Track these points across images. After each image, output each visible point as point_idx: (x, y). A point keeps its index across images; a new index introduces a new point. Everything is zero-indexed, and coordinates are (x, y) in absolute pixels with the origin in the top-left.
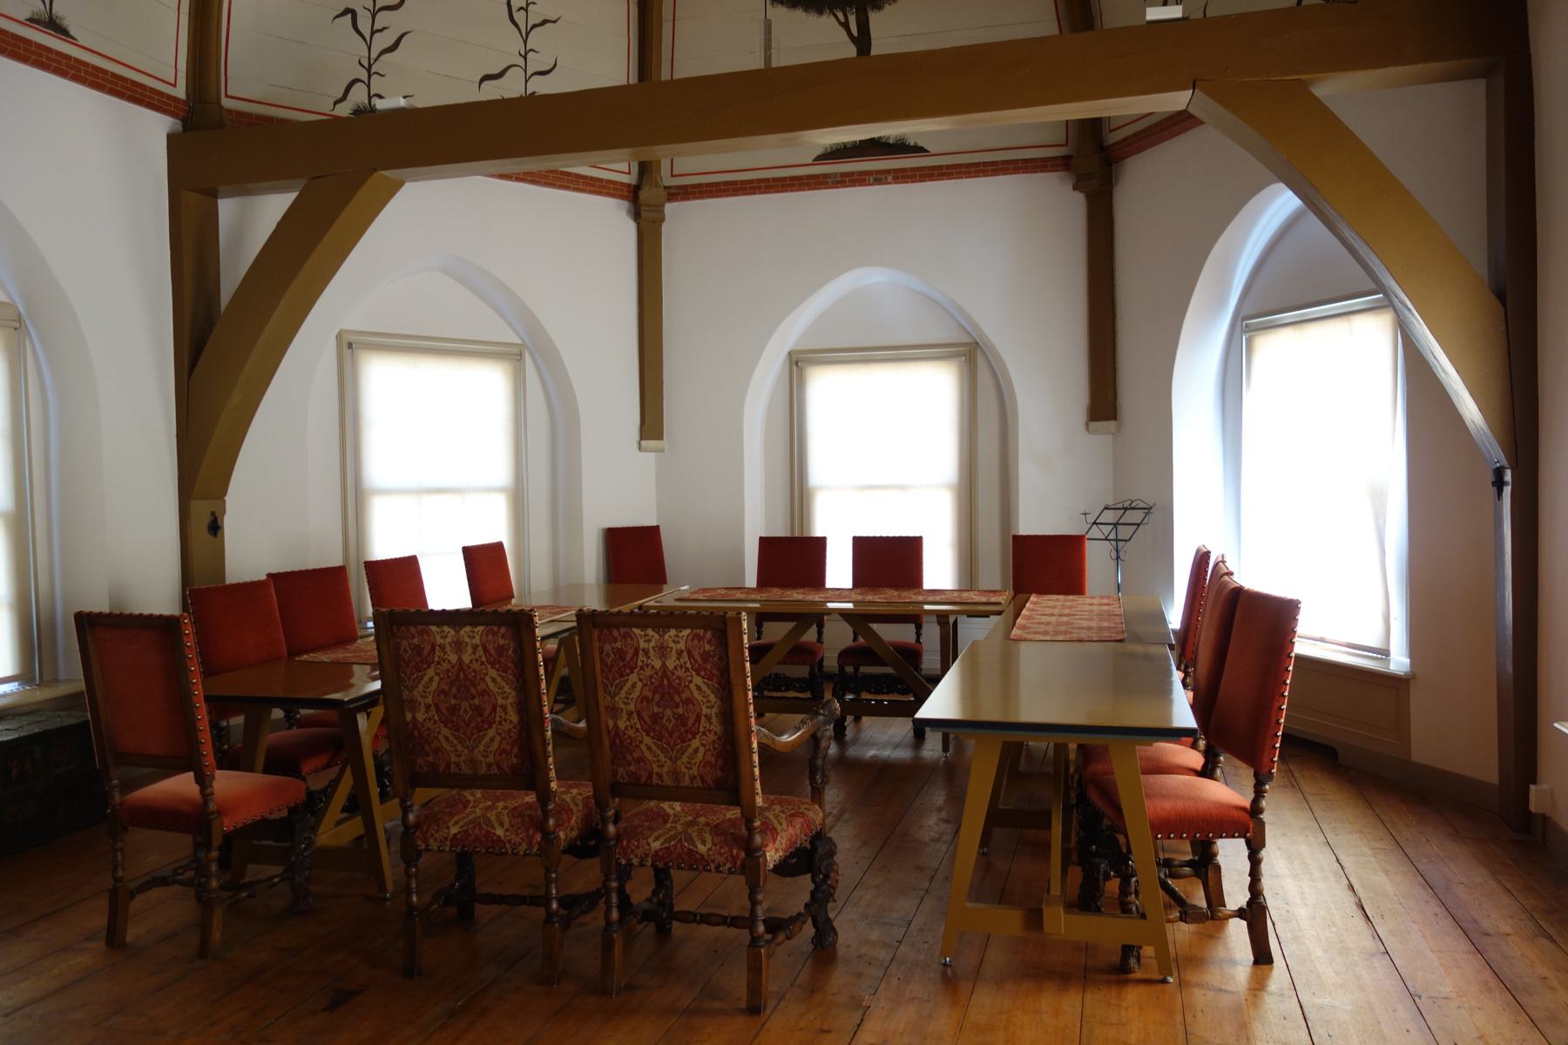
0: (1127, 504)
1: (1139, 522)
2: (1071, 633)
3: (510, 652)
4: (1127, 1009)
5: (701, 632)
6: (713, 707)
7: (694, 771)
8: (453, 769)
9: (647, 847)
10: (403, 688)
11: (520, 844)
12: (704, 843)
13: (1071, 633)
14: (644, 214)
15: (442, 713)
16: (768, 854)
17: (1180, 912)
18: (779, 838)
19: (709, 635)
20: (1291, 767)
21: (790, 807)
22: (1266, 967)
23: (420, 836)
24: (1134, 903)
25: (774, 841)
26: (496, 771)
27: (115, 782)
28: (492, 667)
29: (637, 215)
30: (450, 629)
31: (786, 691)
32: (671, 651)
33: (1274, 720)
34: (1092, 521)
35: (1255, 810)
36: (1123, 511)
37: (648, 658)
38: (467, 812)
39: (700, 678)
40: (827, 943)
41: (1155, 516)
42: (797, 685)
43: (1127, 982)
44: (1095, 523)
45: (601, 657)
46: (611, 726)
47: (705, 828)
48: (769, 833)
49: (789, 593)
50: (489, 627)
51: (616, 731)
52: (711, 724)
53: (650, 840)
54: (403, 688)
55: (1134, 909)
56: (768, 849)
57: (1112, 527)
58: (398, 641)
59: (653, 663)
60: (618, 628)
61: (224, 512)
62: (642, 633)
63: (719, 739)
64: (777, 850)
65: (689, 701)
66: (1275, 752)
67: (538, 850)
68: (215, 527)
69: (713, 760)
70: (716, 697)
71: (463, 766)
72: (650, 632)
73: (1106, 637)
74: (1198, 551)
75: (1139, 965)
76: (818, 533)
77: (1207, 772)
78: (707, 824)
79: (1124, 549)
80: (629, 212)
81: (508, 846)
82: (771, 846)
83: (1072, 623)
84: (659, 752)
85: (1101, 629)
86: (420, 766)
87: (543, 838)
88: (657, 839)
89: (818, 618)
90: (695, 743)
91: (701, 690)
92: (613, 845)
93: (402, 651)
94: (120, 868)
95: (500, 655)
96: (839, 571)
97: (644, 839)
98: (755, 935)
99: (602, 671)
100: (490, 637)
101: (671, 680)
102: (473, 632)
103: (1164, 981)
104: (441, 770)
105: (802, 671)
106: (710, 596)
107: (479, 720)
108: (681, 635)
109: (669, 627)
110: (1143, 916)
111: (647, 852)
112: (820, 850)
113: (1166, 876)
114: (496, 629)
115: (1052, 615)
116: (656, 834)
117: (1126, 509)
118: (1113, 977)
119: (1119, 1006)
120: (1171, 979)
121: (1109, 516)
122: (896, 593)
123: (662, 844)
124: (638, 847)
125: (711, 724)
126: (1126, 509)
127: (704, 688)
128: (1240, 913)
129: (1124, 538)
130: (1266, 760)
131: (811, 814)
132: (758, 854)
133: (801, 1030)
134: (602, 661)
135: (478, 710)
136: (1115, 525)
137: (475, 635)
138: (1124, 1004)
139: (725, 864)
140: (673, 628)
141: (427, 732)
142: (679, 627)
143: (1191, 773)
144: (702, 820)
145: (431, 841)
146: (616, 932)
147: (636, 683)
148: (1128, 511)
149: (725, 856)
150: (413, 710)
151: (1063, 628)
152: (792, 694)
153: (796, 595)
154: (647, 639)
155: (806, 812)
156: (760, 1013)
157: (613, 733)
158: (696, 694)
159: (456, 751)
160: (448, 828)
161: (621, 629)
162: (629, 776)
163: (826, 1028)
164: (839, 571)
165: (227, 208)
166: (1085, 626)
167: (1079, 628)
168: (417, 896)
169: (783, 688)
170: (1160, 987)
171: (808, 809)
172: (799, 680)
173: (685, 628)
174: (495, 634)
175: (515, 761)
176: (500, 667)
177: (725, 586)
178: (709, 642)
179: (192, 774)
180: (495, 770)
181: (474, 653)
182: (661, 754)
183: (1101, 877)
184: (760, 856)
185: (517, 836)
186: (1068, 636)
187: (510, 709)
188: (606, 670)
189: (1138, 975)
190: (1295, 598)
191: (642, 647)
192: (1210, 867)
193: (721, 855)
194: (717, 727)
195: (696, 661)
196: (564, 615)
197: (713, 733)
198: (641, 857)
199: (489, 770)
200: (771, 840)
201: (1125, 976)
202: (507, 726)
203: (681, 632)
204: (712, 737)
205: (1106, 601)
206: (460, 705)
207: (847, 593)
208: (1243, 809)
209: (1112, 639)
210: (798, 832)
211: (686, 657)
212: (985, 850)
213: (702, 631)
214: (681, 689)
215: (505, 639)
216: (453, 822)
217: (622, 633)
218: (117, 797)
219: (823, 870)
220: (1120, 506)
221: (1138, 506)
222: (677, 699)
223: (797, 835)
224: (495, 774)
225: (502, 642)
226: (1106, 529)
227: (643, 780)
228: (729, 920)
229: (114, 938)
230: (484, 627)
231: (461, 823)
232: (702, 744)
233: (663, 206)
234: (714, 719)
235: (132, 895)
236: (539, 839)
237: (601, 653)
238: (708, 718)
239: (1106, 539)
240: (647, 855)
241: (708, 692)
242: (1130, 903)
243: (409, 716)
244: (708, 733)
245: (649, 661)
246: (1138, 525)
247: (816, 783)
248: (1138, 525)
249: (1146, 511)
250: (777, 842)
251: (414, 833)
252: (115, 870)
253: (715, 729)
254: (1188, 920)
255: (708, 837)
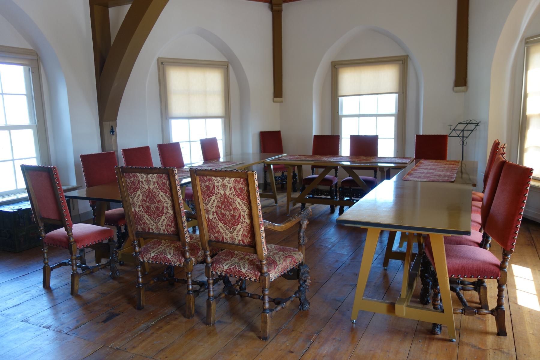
0: (468, 122)
1: (473, 129)
2: (431, 177)
3: (167, 185)
4: (430, 354)
5: (239, 179)
6: (245, 212)
7: (240, 238)
8: (151, 231)
9: (222, 268)
10: (130, 198)
11: (177, 262)
12: (244, 268)
13: (431, 177)
14: (274, 8)
15: (144, 209)
16: (271, 275)
17: (462, 310)
18: (277, 267)
19: (242, 181)
20: (533, 236)
21: (287, 253)
22: (503, 337)
23: (140, 256)
24: (439, 305)
25: (275, 268)
26: (167, 232)
27: (41, 228)
28: (161, 191)
29: (272, 9)
30: (144, 175)
31: (321, 195)
32: (227, 187)
33: (514, 225)
34: (453, 129)
35: (501, 267)
36: (466, 125)
37: (219, 189)
38: (159, 247)
39: (147, 215)
40: (305, 308)
41: (481, 127)
42: (325, 193)
43: (433, 339)
44: (454, 130)
45: (201, 188)
46: (207, 217)
47: (246, 261)
48: (273, 265)
49: (323, 157)
50: (158, 175)
51: (209, 219)
52: (245, 219)
53: (224, 265)
54: (130, 198)
55: (439, 307)
56: (271, 272)
57: (461, 131)
58: (126, 179)
59: (220, 192)
60: (206, 176)
61: (116, 126)
62: (216, 179)
63: (248, 225)
64: (276, 273)
65: (235, 209)
66: (515, 241)
67: (183, 265)
68: (113, 131)
69: (246, 234)
70: (246, 207)
71: (154, 230)
72: (218, 178)
73: (446, 180)
74: (495, 142)
75: (441, 331)
76: (174, 140)
77: (482, 245)
78: (248, 259)
79: (465, 141)
80: (269, 7)
81: (172, 263)
82: (273, 271)
83: (433, 173)
84: (225, 229)
85: (445, 176)
86: (139, 229)
87: (185, 261)
88: (227, 265)
89: (335, 167)
90: (239, 226)
91: (240, 204)
92: (210, 266)
93: (128, 183)
94: (46, 259)
95: (164, 186)
96: (345, 149)
97: (222, 264)
98: (264, 308)
99: (202, 194)
100: (159, 179)
101: (228, 199)
102: (152, 176)
103: (451, 341)
104: (147, 231)
105: (326, 188)
106: (292, 158)
107: (158, 212)
108: (231, 180)
109: (226, 177)
110: (443, 312)
111: (223, 270)
112: (302, 270)
113: (460, 290)
114: (161, 175)
115: (426, 169)
116: (227, 262)
117: (468, 124)
118: (428, 336)
119: (427, 352)
120: (454, 340)
121: (461, 127)
122: (365, 158)
123: (228, 267)
124: (219, 267)
125: (245, 219)
126: (468, 124)
127: (241, 203)
128: (492, 312)
129: (466, 136)
130: (509, 244)
131: (296, 256)
132: (266, 275)
133: (281, 350)
134: (201, 190)
135: (157, 208)
136: (463, 131)
137: (154, 177)
138: (429, 351)
139: (252, 278)
140: (227, 177)
141: (140, 216)
142: (230, 177)
143: (476, 244)
144: (247, 257)
145: (145, 259)
146: (212, 300)
147: (214, 200)
148: (469, 125)
149: (253, 274)
150: (134, 207)
151: (428, 175)
152: (323, 197)
153: (325, 159)
154: (217, 181)
155: (294, 255)
156: (266, 340)
157: (207, 220)
158: (238, 205)
159: (151, 224)
160: (150, 254)
161: (207, 177)
162: (215, 238)
163: (292, 350)
164: (345, 149)
165: (112, 11)
166: (438, 174)
167: (435, 175)
168: (139, 281)
169: (320, 194)
170: (449, 343)
171: (295, 254)
172: (326, 191)
173: (232, 177)
174: (161, 177)
175: (173, 229)
176: (164, 191)
177: (299, 155)
178: (242, 184)
179: (64, 228)
180: (166, 232)
181: (230, 190)
182: (226, 230)
183: (430, 288)
184: (266, 276)
185: (175, 259)
186: (429, 179)
187: (169, 208)
188: (203, 194)
189: (439, 336)
190: (530, 167)
191: (216, 185)
192: (481, 287)
193: (251, 274)
194: (248, 221)
195: (237, 192)
196: (230, 166)
197: (246, 222)
198: (221, 272)
199: (164, 232)
200: (273, 269)
201: (433, 336)
202: (169, 215)
203: (231, 179)
204: (245, 224)
205: (453, 163)
206: (150, 206)
207: (345, 158)
208: (496, 265)
209: (448, 181)
210: (288, 264)
211: (233, 190)
212: (386, 268)
213: (239, 179)
214: (141, 219)
215: (165, 180)
216: (152, 251)
217: (208, 179)
218: (43, 234)
219: (303, 279)
220: (465, 122)
221: (473, 123)
222: (231, 208)
223: (288, 265)
224: (166, 234)
225: (164, 181)
226: (458, 132)
227: (220, 240)
228: (261, 297)
229: (46, 285)
230: (157, 174)
231: (156, 252)
232: (242, 227)
233: (282, 4)
234: (246, 217)
235: (52, 269)
236: (183, 261)
237: (201, 187)
238: (244, 216)
239: (458, 136)
240: (223, 271)
241: (243, 205)
242: (438, 305)
243: (133, 210)
244: (244, 223)
245: (219, 191)
246: (472, 131)
247: (300, 243)
248: (472, 131)
249: (476, 125)
250: (276, 269)
251: (139, 255)
252: (44, 260)
253: (247, 221)
254: (465, 314)
255: (247, 266)
